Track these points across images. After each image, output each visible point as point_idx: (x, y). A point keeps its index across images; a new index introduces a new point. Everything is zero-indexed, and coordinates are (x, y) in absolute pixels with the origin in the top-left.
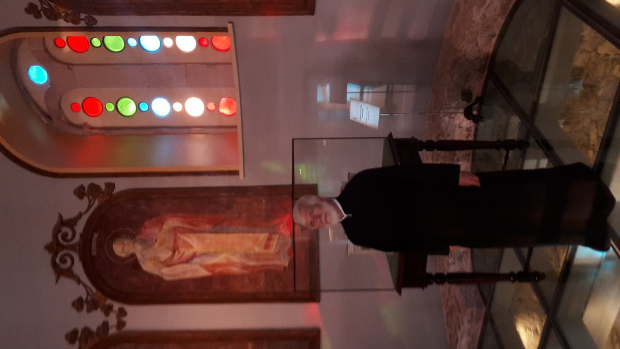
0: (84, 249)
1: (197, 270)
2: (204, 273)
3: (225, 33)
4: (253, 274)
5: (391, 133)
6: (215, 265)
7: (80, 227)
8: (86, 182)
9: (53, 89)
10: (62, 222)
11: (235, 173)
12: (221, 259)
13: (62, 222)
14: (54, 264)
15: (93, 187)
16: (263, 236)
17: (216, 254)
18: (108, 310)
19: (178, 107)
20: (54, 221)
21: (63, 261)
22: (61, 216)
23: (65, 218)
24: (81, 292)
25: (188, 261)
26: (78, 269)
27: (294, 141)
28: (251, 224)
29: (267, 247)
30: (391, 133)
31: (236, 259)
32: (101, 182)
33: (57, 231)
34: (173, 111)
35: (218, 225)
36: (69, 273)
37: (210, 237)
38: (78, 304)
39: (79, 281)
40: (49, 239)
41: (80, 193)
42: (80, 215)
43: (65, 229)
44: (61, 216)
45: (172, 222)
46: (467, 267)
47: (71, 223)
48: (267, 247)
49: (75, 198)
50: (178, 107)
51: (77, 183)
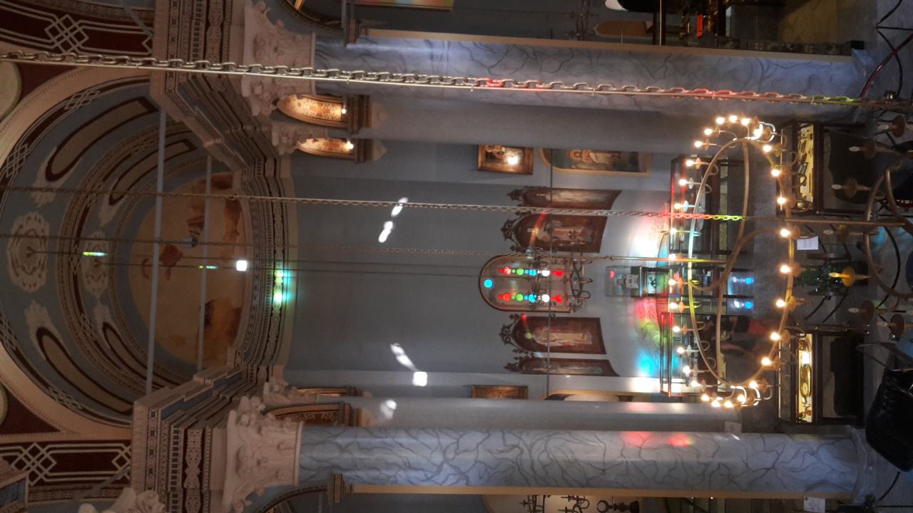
0: (514, 335)
1: (557, 344)
2: (560, 345)
4: (580, 346)
5: (509, 195)
7: (512, 329)
8: (513, 313)
9: (493, 290)
10: (504, 327)
12: (566, 341)
13: (504, 327)
16: (581, 335)
18: (527, 353)
20: (501, 326)
23: (506, 325)
24: (514, 244)
25: (554, 341)
26: (513, 341)
28: (576, 330)
29: (583, 338)
30: (509, 195)
31: (572, 341)
32: (519, 313)
33: (502, 330)
35: (563, 330)
36: (509, 342)
38: (512, 248)
39: (514, 345)
40: (500, 332)
41: (511, 317)
42: (516, 220)
45: (546, 329)
47: (508, 327)
48: (583, 338)
49: (510, 319)
51: (510, 313)
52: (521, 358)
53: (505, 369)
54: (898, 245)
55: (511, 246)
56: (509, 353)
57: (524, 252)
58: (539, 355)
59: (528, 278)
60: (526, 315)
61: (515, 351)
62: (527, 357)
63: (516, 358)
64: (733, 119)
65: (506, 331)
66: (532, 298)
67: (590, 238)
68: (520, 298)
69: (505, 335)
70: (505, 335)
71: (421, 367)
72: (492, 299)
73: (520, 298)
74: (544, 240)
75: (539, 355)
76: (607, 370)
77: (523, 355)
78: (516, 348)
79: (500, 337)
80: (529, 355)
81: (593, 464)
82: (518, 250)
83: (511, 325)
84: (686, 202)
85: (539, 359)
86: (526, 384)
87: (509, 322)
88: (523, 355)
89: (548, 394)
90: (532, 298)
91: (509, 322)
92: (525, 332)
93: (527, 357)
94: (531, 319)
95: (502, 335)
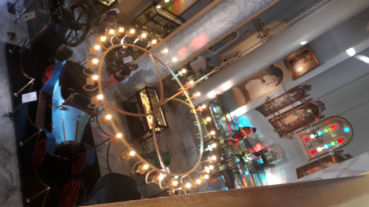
0: (317, 107)
3: (250, 101)
6: (290, 116)
7: (320, 110)
8: (324, 119)
9: (342, 128)
11: (296, 133)
14: (321, 102)
15: (321, 118)
17: (292, 118)
18: (305, 101)
19: (330, 145)
20: (326, 108)
21: (320, 103)
22: (269, 123)
23: (324, 111)
26: (316, 104)
27: (247, 87)
32: (321, 120)
33: (324, 107)
34: (330, 144)
36: (317, 102)
37: (294, 120)
40: (325, 105)
41: (324, 116)
43: (323, 108)
44: (269, 123)
46: (225, 146)
47: (322, 110)
50: (330, 145)
52: (306, 96)
53: (309, 84)
54: (104, 141)
55: (344, 152)
56: (314, 95)
57: (335, 152)
58: (299, 103)
59: (328, 143)
60: (317, 121)
61: (311, 99)
62: (304, 99)
63: (309, 95)
64: (199, 182)
65: (322, 107)
66: (320, 133)
67: (303, 174)
68: (326, 131)
69: (321, 105)
70: (321, 105)
71: (352, 59)
72: (340, 123)
73: (326, 131)
74: (327, 163)
75: (299, 103)
76: (261, 109)
77: (306, 99)
78: (312, 101)
79: (323, 102)
80: (303, 100)
81: (220, 10)
82: (339, 152)
83: (321, 112)
84: (182, 75)
85: (298, 100)
86: (295, 81)
87: (323, 113)
88: (306, 99)
89: (282, 84)
90: (320, 133)
91: (323, 113)
92: (312, 112)
93: (304, 99)
94: (314, 120)
95: (323, 105)
